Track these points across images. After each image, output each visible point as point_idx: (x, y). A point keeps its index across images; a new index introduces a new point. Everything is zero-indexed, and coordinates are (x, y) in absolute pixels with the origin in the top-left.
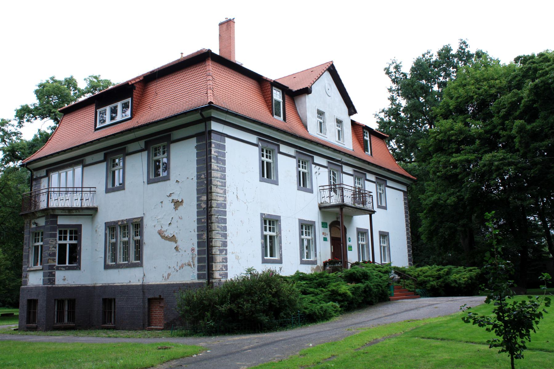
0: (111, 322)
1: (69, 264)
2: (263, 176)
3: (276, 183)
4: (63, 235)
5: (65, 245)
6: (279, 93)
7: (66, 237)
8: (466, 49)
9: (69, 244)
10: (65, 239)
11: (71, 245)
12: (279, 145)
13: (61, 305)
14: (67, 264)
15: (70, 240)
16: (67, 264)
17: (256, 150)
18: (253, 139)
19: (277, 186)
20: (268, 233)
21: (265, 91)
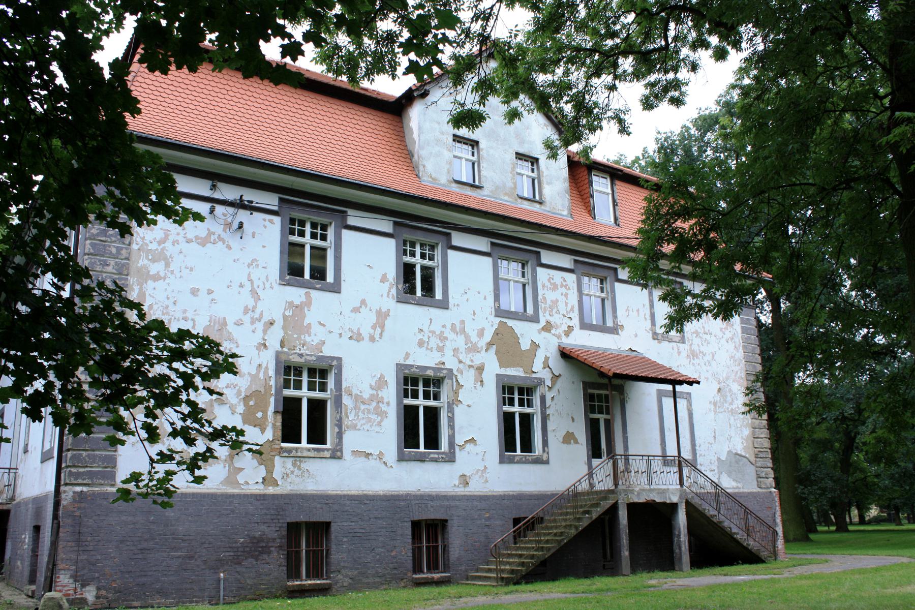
0: (322, 576)
1: (425, 448)
2: (412, 290)
3: (444, 305)
4: (596, 404)
5: (299, 400)
6: (605, 180)
7: (513, 399)
8: (504, 108)
9: (425, 408)
10: (415, 396)
11: (311, 401)
12: (539, 253)
13: (608, 547)
14: (422, 448)
15: (424, 398)
16: (422, 448)
17: (390, 245)
18: (386, 225)
19: (445, 311)
20: (516, 409)
21: (577, 177)
